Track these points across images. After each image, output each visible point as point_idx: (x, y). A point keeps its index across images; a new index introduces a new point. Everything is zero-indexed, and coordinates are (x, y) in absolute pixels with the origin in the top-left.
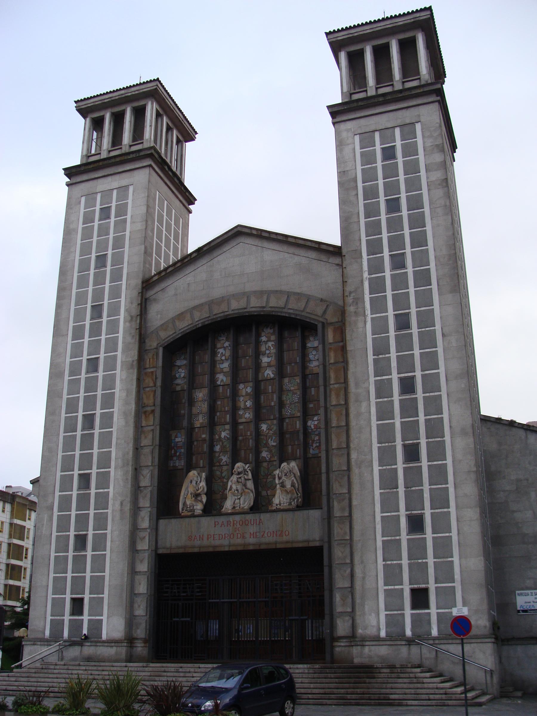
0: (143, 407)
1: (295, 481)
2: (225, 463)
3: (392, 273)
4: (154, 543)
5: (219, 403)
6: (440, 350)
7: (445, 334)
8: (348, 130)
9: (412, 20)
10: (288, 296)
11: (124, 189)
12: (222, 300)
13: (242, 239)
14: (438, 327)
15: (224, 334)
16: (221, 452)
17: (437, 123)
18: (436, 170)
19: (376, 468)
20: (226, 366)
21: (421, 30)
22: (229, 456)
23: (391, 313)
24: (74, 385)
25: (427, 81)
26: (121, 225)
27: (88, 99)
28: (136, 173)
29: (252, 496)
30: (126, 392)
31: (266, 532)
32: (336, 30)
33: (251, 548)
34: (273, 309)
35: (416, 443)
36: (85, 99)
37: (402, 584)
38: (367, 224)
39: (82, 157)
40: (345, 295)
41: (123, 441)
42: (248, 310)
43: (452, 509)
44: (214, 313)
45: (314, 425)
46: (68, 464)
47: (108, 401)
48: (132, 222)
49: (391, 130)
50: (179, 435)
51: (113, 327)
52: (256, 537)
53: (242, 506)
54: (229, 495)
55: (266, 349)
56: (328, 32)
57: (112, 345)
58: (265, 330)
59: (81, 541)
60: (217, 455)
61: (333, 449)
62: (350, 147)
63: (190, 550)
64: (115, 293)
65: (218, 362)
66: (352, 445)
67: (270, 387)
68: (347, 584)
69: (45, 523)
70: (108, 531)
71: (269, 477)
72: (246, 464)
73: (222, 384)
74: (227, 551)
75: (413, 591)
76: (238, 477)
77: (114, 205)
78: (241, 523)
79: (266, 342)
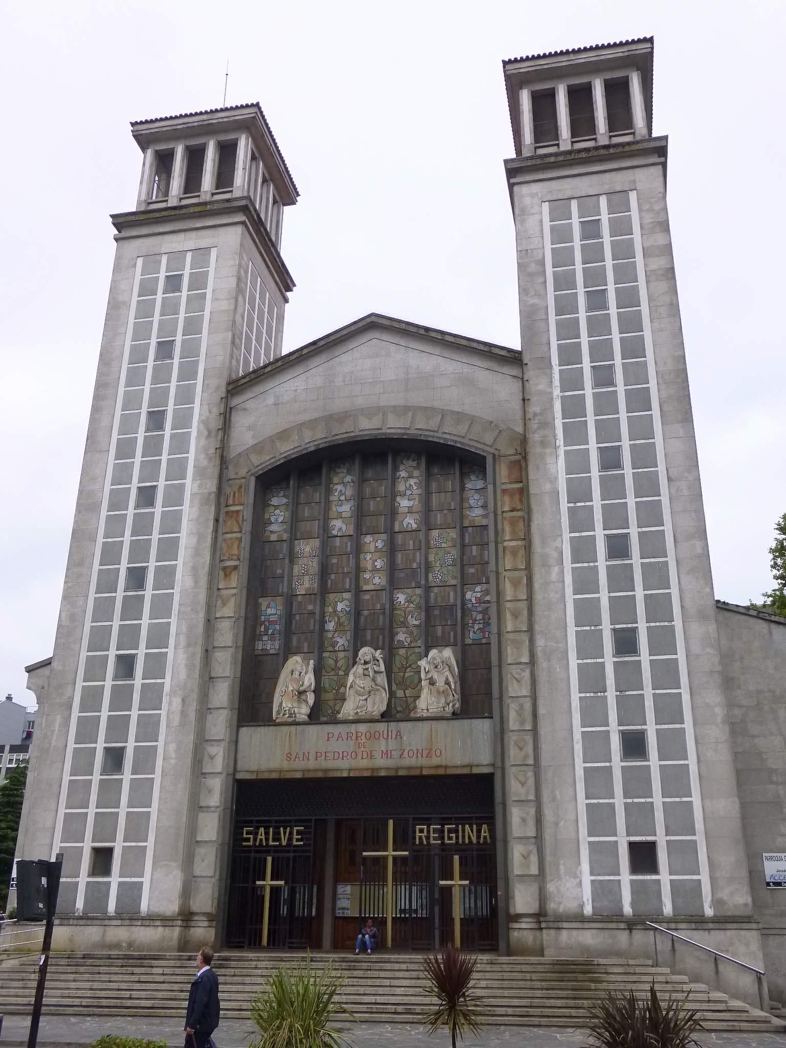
0: (222, 561)
1: (451, 679)
3: (595, 391)
6: (665, 499)
7: (673, 477)
8: (533, 195)
9: (626, 54)
10: (443, 415)
11: (202, 253)
12: (344, 416)
13: (376, 334)
14: (661, 468)
15: (344, 464)
17: (660, 193)
18: (657, 256)
19: (574, 662)
20: (346, 509)
21: (635, 69)
22: (348, 638)
23: (593, 446)
24: (115, 524)
25: (645, 136)
26: (197, 302)
27: (152, 121)
28: (222, 231)
29: (385, 696)
30: (197, 537)
31: (406, 751)
32: (519, 59)
33: (383, 773)
34: (420, 432)
35: (632, 628)
36: (147, 122)
37: (615, 835)
38: (558, 323)
39: (139, 203)
40: (527, 418)
41: (189, 609)
42: (383, 431)
43: (688, 725)
46: (99, 640)
47: (169, 549)
48: (215, 299)
49: (594, 198)
50: (272, 604)
51: (180, 443)
53: (369, 709)
54: (350, 694)
55: (407, 489)
56: (507, 60)
57: (177, 470)
58: (404, 462)
59: (115, 758)
61: (508, 632)
62: (537, 217)
64: (185, 396)
66: (537, 628)
67: (411, 542)
68: (531, 831)
69: (57, 729)
70: (160, 744)
72: (376, 649)
74: (345, 778)
75: (632, 845)
76: (364, 667)
77: (187, 272)
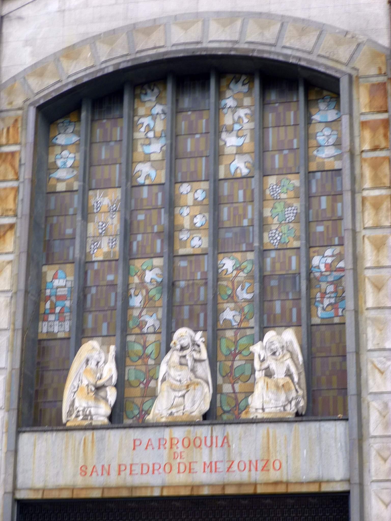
2: (151, 330)
4: (10, 479)
5: (141, 217)
10: (282, 25)
15: (153, 90)
16: (144, 308)
29: (208, 391)
33: (205, 492)
44: (137, 50)
45: (326, 265)
52: (216, 471)
60: (136, 313)
63: (83, 495)
65: (139, 142)
67: (241, 193)
71: (237, 358)
72: (196, 331)
73: (147, 182)
78: (186, 443)
79: (234, 109)
